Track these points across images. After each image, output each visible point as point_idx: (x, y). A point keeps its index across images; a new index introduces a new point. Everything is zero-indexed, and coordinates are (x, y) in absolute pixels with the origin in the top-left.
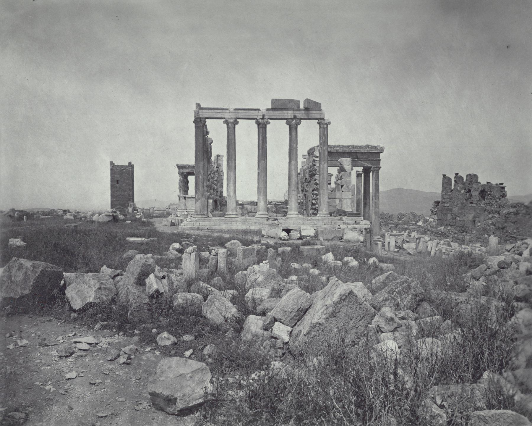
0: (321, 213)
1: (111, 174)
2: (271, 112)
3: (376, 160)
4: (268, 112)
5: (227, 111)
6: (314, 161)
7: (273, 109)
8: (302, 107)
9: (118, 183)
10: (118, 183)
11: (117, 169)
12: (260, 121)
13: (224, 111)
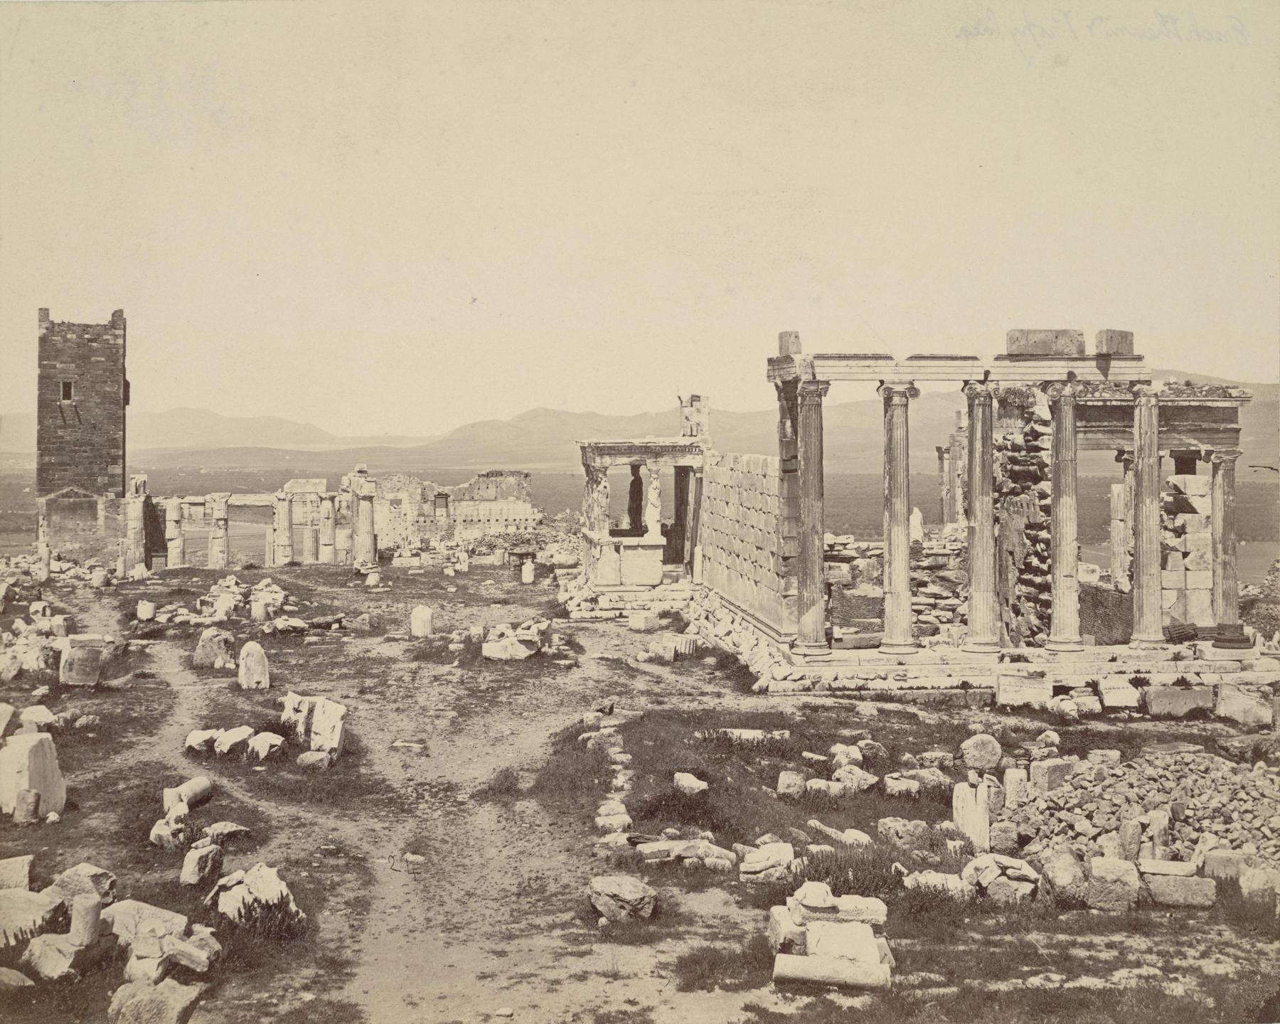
0: (1144, 637)
1: (41, 358)
2: (1007, 363)
3: (1226, 431)
4: (998, 363)
5: (889, 362)
6: (1037, 435)
7: (1012, 357)
8: (1091, 350)
9: (67, 395)
10: (67, 395)
11: (66, 340)
12: (979, 388)
13: (880, 362)
